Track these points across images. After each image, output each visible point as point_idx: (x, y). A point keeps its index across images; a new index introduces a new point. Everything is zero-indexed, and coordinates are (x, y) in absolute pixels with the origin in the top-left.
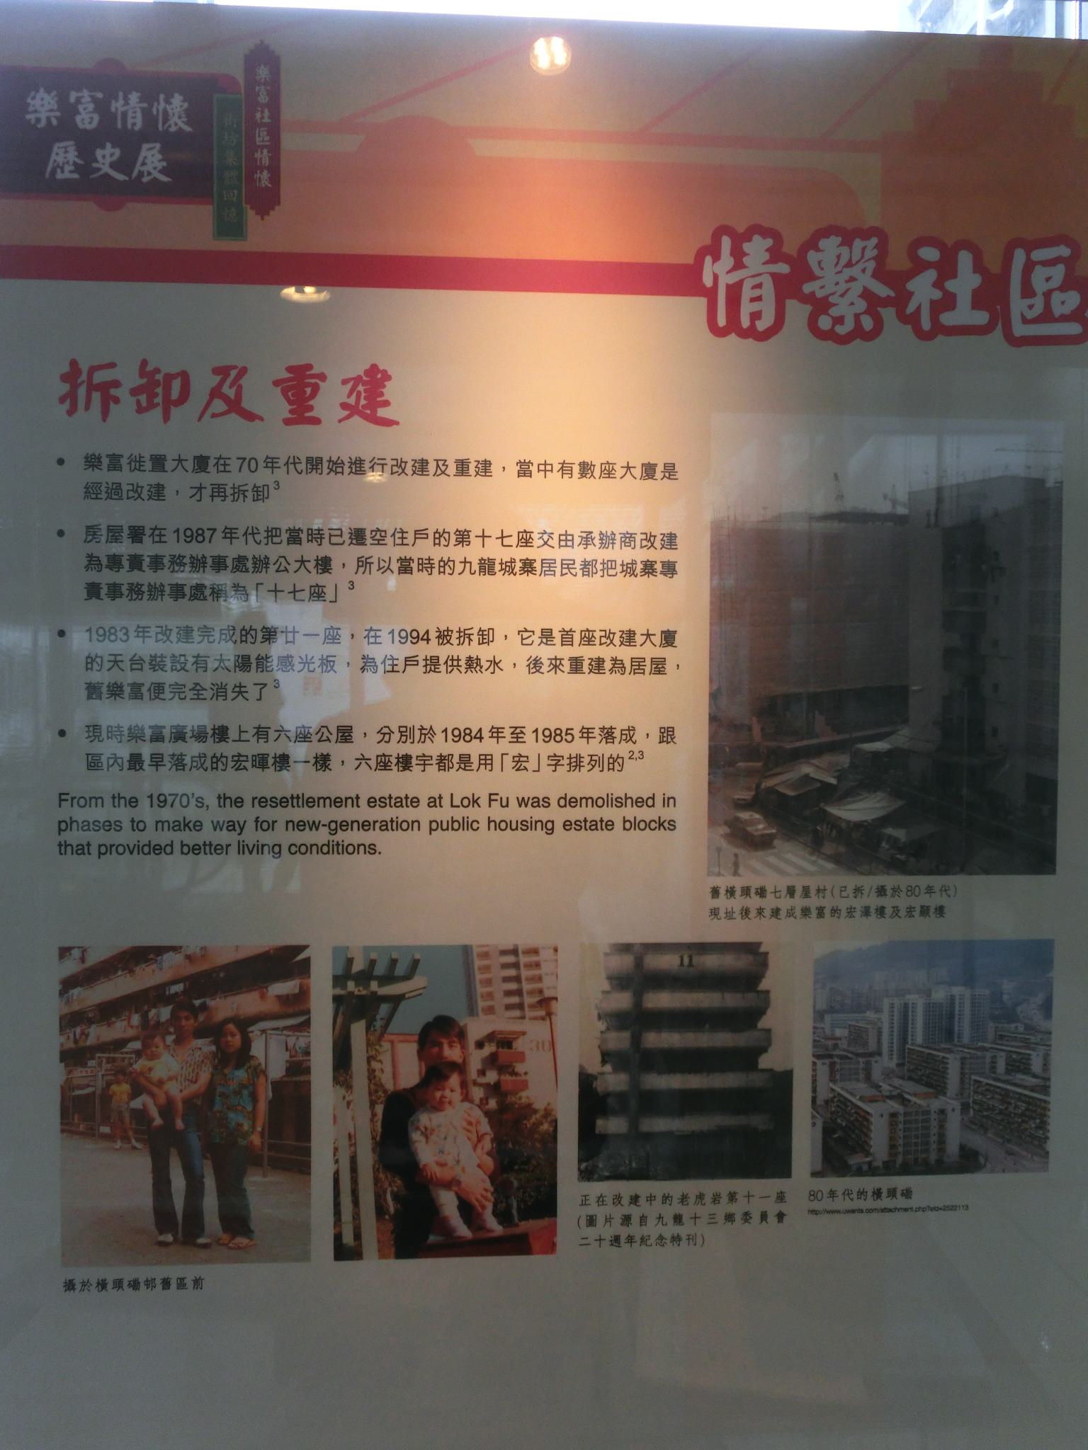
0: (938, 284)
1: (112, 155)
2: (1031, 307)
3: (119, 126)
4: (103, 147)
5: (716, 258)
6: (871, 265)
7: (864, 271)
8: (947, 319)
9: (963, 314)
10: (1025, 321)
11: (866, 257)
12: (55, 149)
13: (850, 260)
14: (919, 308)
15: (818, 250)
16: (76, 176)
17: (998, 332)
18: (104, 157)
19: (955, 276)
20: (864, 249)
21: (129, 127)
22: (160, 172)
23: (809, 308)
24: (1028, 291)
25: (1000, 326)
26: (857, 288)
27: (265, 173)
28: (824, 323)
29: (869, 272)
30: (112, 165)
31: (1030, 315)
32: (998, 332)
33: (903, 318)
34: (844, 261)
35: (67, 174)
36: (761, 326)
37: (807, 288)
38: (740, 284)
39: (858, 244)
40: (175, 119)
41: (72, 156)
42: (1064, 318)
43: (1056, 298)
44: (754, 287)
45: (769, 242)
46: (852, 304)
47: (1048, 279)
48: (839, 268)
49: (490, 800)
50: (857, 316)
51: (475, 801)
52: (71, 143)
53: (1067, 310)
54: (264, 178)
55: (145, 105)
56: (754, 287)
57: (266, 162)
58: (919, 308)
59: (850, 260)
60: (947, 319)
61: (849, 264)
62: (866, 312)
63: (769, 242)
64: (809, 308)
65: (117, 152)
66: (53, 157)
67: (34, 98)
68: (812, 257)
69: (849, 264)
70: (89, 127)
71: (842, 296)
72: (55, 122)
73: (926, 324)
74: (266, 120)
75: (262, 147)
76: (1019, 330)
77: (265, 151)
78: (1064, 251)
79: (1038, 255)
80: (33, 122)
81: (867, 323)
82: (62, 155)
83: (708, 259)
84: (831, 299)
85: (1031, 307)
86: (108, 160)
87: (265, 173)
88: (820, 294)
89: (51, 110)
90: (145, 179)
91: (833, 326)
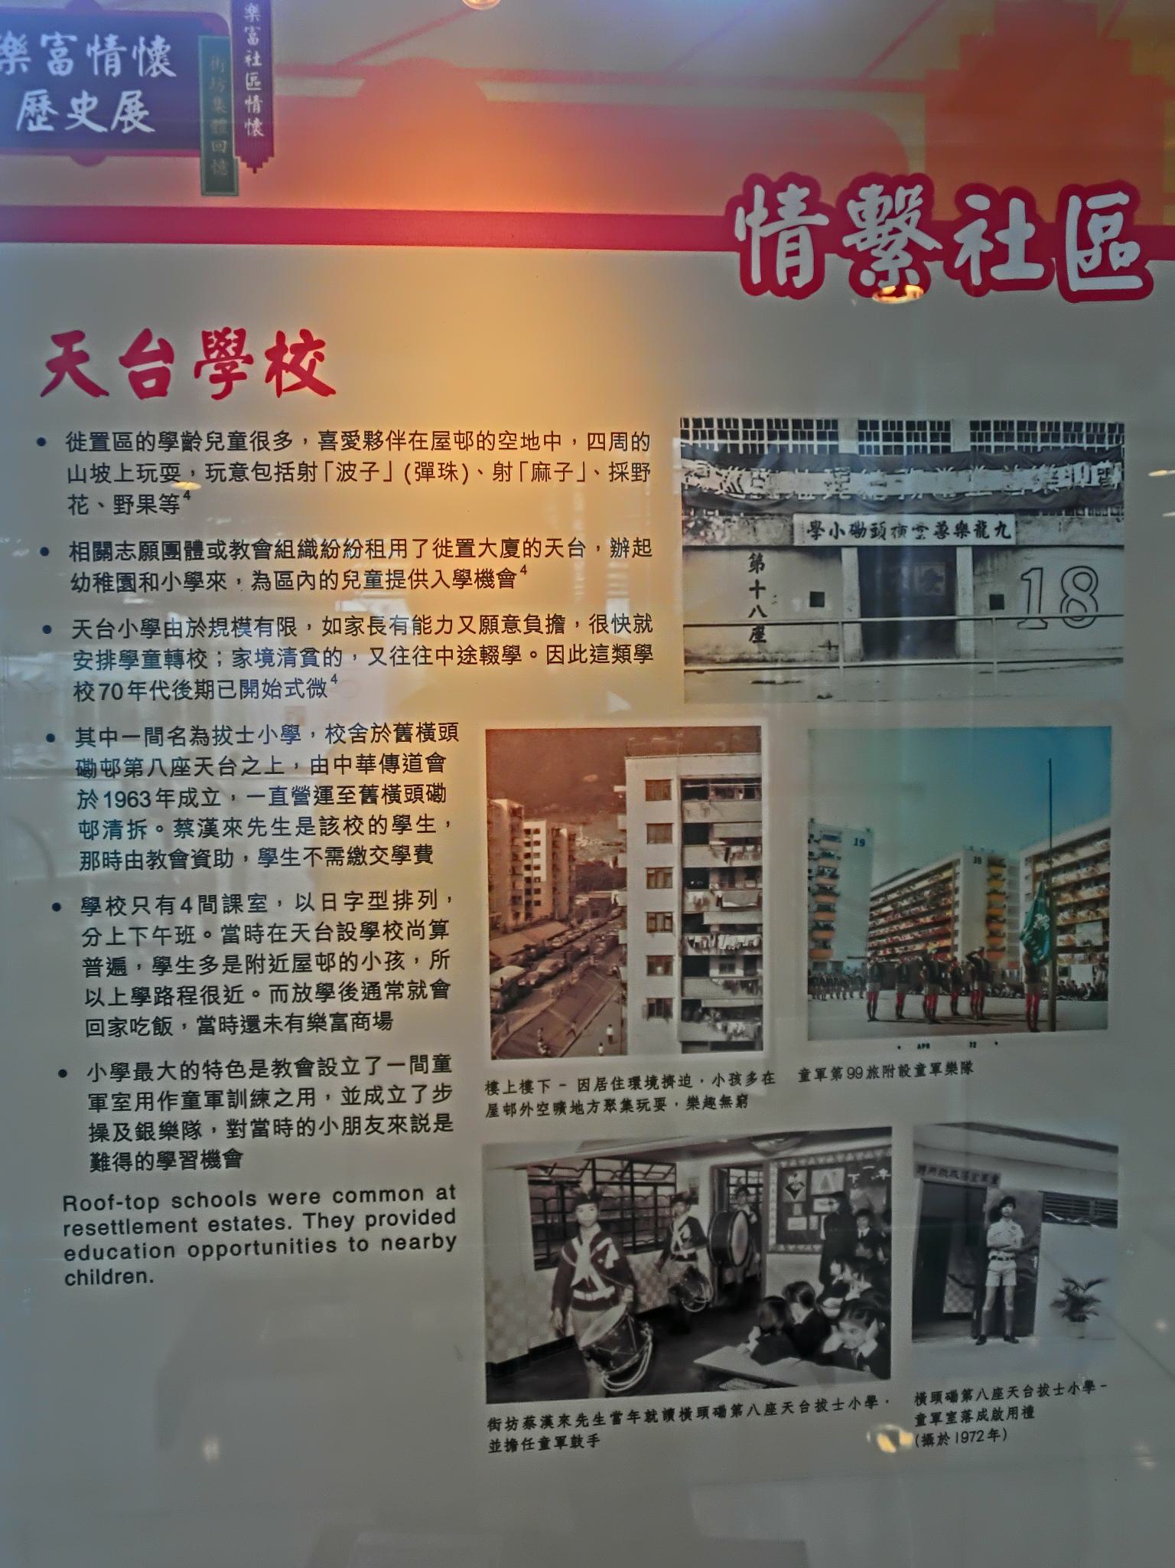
0: (988, 235)
1: (89, 104)
2: (1088, 259)
4: (79, 96)
5: (749, 210)
7: (908, 221)
8: (998, 272)
10: (1082, 274)
12: (26, 99)
15: (859, 200)
18: (80, 106)
20: (908, 198)
21: (107, 72)
23: (850, 263)
24: (1084, 242)
26: (901, 241)
30: (90, 116)
33: (950, 272)
34: (886, 211)
36: (799, 282)
40: (157, 63)
42: (1122, 271)
43: (1114, 249)
44: (790, 241)
45: (805, 192)
46: (896, 258)
47: (1105, 229)
48: (881, 219)
52: (44, 91)
56: (790, 241)
57: (258, 109)
60: (998, 272)
63: (805, 192)
65: (95, 101)
66: (24, 107)
68: (852, 207)
69: (893, 215)
71: (886, 249)
73: (976, 279)
74: (257, 64)
75: (253, 93)
76: (1076, 284)
78: (1122, 198)
79: (1094, 203)
85: (1088, 259)
86: (85, 110)
88: (861, 247)
89: (21, 56)
90: (126, 130)
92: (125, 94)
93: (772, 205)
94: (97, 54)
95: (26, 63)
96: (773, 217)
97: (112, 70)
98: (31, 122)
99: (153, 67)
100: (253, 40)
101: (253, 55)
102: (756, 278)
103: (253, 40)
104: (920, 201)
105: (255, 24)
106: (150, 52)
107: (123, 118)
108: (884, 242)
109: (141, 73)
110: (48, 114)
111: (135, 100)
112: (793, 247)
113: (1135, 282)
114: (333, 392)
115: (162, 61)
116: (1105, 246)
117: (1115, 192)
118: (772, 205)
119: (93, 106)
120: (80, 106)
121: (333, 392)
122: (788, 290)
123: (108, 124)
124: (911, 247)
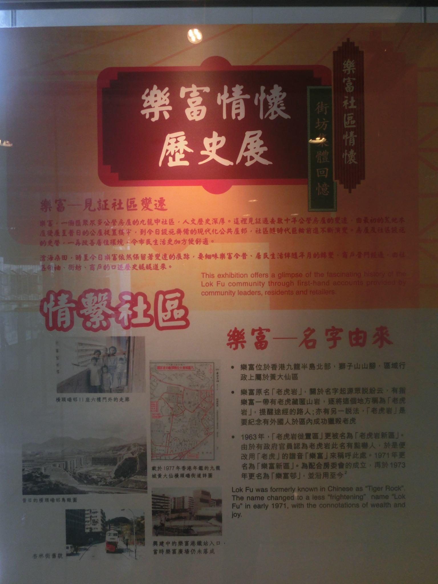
0: (131, 309)
1: (218, 143)
2: (166, 316)
3: (225, 117)
4: (210, 136)
5: (48, 302)
6: (105, 303)
7: (102, 305)
8: (134, 321)
9: (141, 319)
10: (164, 321)
11: (103, 300)
12: (167, 140)
13: (97, 301)
14: (123, 318)
15: (85, 298)
16: (186, 163)
17: (154, 325)
18: (211, 145)
19: (137, 305)
20: (102, 297)
21: (234, 117)
22: (262, 156)
23: (82, 319)
24: (165, 310)
25: (154, 323)
26: (100, 311)
27: (352, 152)
28: (89, 324)
29: (105, 305)
30: (219, 152)
31: (166, 319)
32: (154, 325)
33: (118, 321)
34: (95, 301)
35: (178, 162)
36: (65, 326)
37: (82, 312)
38: (57, 311)
39: (100, 295)
40: (275, 108)
41: (183, 145)
42: (178, 319)
43: (175, 312)
44: (62, 312)
45: (67, 296)
46: (99, 317)
47: (172, 305)
48: (93, 304)
49: (246, 489)
50: (101, 322)
51: (241, 490)
52: (183, 133)
53: (180, 316)
54: (351, 156)
55: (247, 97)
56: (62, 312)
57: (352, 142)
58: (123, 318)
59: (97, 301)
60: (134, 321)
61: (97, 303)
62: (104, 320)
63: (67, 296)
64: (82, 319)
65: (223, 139)
66: (165, 147)
67: (148, 95)
68: (83, 300)
69: (97, 303)
70: (198, 119)
71: (95, 314)
72: (167, 116)
73: (126, 323)
74: (352, 107)
75: (349, 130)
76: (162, 324)
77: (352, 133)
78: (178, 295)
79: (168, 296)
80: (147, 117)
81: (105, 324)
82: (173, 145)
83: (45, 303)
84: (91, 316)
85: (166, 316)
86: (215, 147)
87: (352, 152)
88: (86, 314)
89: (164, 105)
90: (248, 164)
91: (92, 325)
92: (248, 134)
93: (56, 301)
94: (226, 102)
95: (168, 111)
96: (56, 304)
97: (238, 115)
98: (170, 159)
99: (272, 111)
100: (349, 88)
101: (349, 99)
102: (51, 325)
103: (349, 88)
104: (107, 298)
105: (351, 76)
106: (269, 98)
107: (245, 154)
108: (94, 312)
109: (261, 117)
110: (185, 152)
111: (257, 138)
112: (63, 314)
113: (183, 323)
114: (392, 343)
115: (279, 106)
116: (172, 311)
117: (176, 292)
118: (56, 301)
119: (221, 145)
120: (211, 145)
121: (392, 343)
122: (62, 329)
123: (234, 160)
124: (104, 313)
